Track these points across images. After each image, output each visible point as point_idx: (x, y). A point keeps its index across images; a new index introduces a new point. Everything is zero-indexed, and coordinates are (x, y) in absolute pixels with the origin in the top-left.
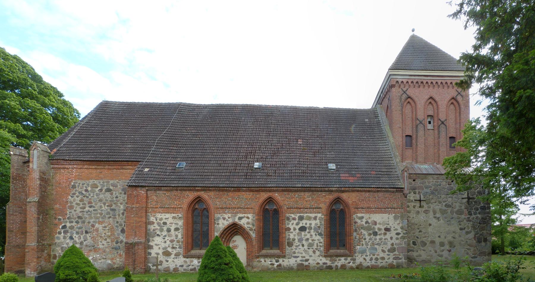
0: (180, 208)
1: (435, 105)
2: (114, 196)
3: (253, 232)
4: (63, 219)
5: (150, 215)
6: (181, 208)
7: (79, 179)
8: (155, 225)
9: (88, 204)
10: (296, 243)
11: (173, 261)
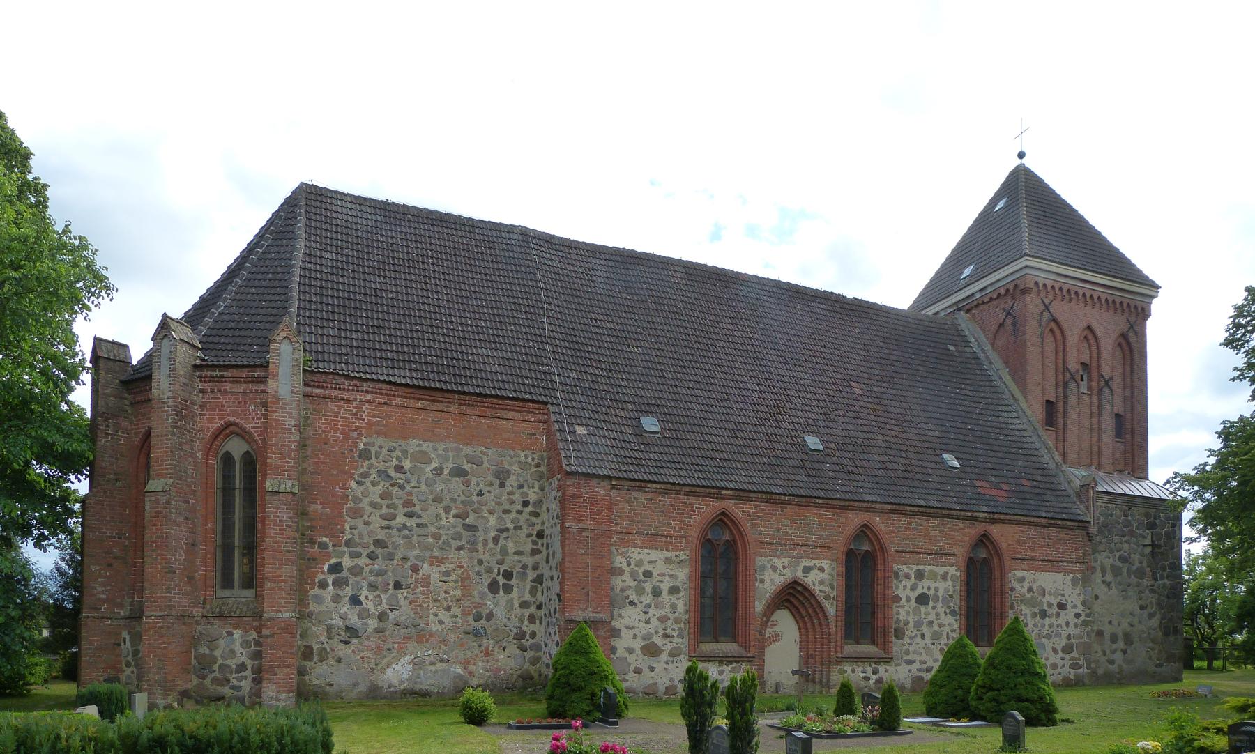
0: (681, 537)
1: (1093, 343)
2: (474, 488)
3: (832, 604)
4: (334, 546)
5: (615, 551)
6: (685, 537)
7: (379, 434)
8: (626, 576)
9: (404, 506)
10: (911, 631)
11: (665, 669)
